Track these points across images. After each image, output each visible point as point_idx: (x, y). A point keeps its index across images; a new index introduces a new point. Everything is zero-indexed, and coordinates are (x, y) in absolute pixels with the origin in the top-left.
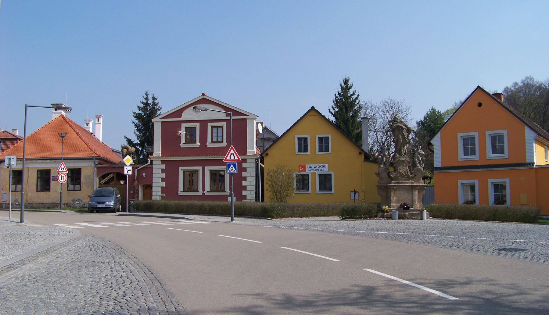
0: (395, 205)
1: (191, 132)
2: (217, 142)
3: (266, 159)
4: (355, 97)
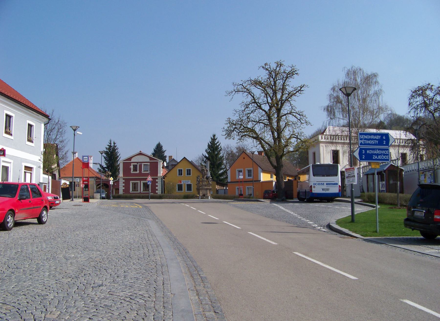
0: (201, 195)
1: (135, 167)
2: (146, 171)
3: (165, 178)
4: (218, 144)
